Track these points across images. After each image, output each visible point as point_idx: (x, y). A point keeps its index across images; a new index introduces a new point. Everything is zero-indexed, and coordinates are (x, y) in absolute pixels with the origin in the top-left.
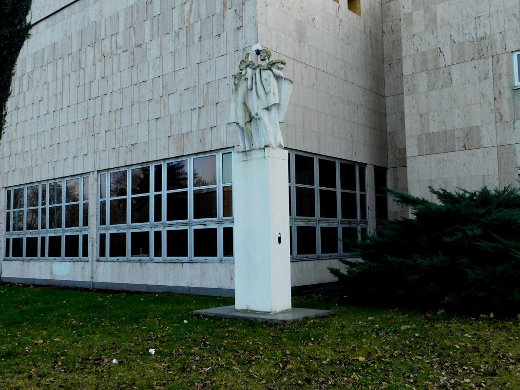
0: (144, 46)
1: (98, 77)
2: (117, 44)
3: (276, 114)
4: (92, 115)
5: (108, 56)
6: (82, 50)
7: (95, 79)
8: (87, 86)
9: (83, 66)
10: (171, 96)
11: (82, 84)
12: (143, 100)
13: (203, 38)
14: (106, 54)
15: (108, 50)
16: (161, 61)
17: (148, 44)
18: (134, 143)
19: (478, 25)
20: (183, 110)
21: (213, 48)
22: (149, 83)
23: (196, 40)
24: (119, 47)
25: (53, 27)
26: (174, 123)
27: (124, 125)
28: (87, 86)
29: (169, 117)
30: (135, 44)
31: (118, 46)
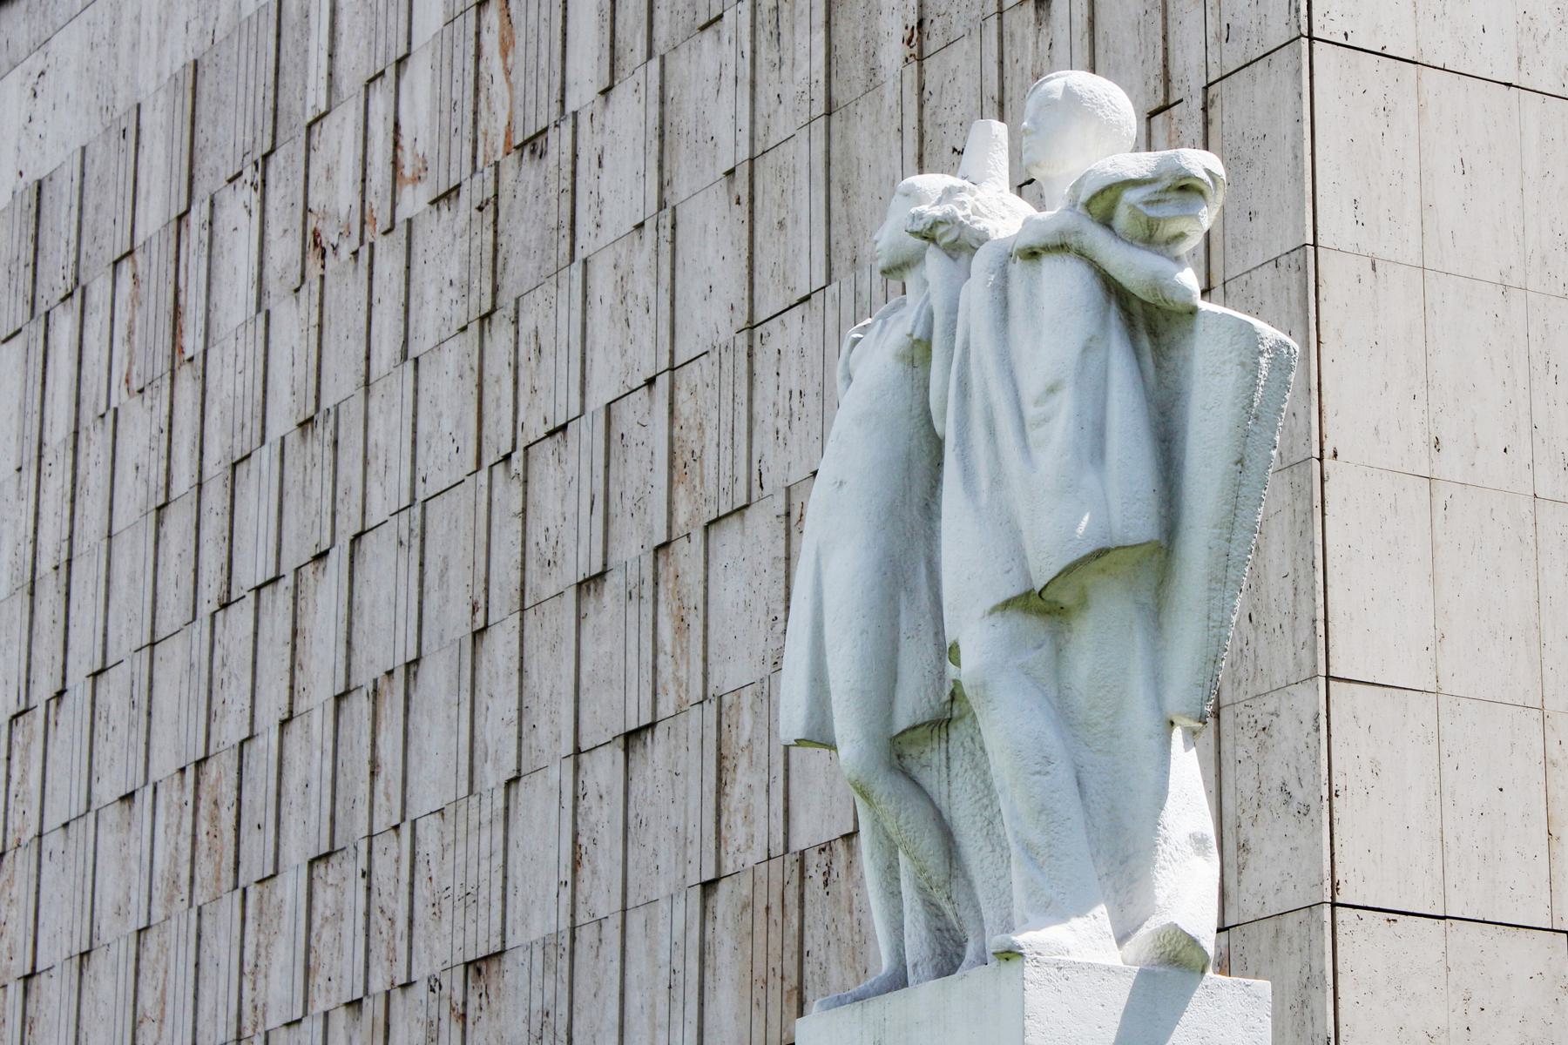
0: (559, 143)
1: (282, 422)
2: (396, 144)
3: (1052, 78)
4: (231, 730)
5: (345, 252)
6: (194, 217)
7: (263, 442)
8: (215, 496)
9: (192, 343)
10: (729, 540)
11: (183, 482)
12: (549, 589)
13: (935, 29)
14: (330, 236)
15: (345, 197)
16: (666, 248)
17: (584, 120)
18: (482, 952)
19: (338, 938)
20: (584, 746)
21: (1321, 459)
22: (588, 434)
23: (893, 53)
24: (408, 170)
25: (36, 63)
26: (743, 762)
27: (422, 803)
28: (215, 496)
29: (711, 710)
30: (509, 133)
31: (407, 159)
